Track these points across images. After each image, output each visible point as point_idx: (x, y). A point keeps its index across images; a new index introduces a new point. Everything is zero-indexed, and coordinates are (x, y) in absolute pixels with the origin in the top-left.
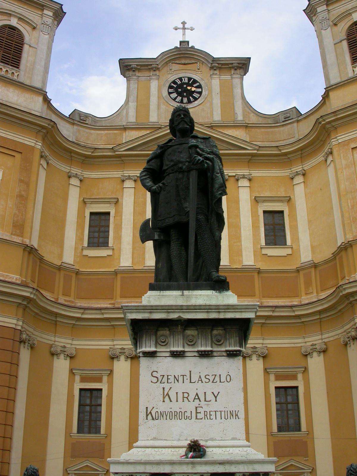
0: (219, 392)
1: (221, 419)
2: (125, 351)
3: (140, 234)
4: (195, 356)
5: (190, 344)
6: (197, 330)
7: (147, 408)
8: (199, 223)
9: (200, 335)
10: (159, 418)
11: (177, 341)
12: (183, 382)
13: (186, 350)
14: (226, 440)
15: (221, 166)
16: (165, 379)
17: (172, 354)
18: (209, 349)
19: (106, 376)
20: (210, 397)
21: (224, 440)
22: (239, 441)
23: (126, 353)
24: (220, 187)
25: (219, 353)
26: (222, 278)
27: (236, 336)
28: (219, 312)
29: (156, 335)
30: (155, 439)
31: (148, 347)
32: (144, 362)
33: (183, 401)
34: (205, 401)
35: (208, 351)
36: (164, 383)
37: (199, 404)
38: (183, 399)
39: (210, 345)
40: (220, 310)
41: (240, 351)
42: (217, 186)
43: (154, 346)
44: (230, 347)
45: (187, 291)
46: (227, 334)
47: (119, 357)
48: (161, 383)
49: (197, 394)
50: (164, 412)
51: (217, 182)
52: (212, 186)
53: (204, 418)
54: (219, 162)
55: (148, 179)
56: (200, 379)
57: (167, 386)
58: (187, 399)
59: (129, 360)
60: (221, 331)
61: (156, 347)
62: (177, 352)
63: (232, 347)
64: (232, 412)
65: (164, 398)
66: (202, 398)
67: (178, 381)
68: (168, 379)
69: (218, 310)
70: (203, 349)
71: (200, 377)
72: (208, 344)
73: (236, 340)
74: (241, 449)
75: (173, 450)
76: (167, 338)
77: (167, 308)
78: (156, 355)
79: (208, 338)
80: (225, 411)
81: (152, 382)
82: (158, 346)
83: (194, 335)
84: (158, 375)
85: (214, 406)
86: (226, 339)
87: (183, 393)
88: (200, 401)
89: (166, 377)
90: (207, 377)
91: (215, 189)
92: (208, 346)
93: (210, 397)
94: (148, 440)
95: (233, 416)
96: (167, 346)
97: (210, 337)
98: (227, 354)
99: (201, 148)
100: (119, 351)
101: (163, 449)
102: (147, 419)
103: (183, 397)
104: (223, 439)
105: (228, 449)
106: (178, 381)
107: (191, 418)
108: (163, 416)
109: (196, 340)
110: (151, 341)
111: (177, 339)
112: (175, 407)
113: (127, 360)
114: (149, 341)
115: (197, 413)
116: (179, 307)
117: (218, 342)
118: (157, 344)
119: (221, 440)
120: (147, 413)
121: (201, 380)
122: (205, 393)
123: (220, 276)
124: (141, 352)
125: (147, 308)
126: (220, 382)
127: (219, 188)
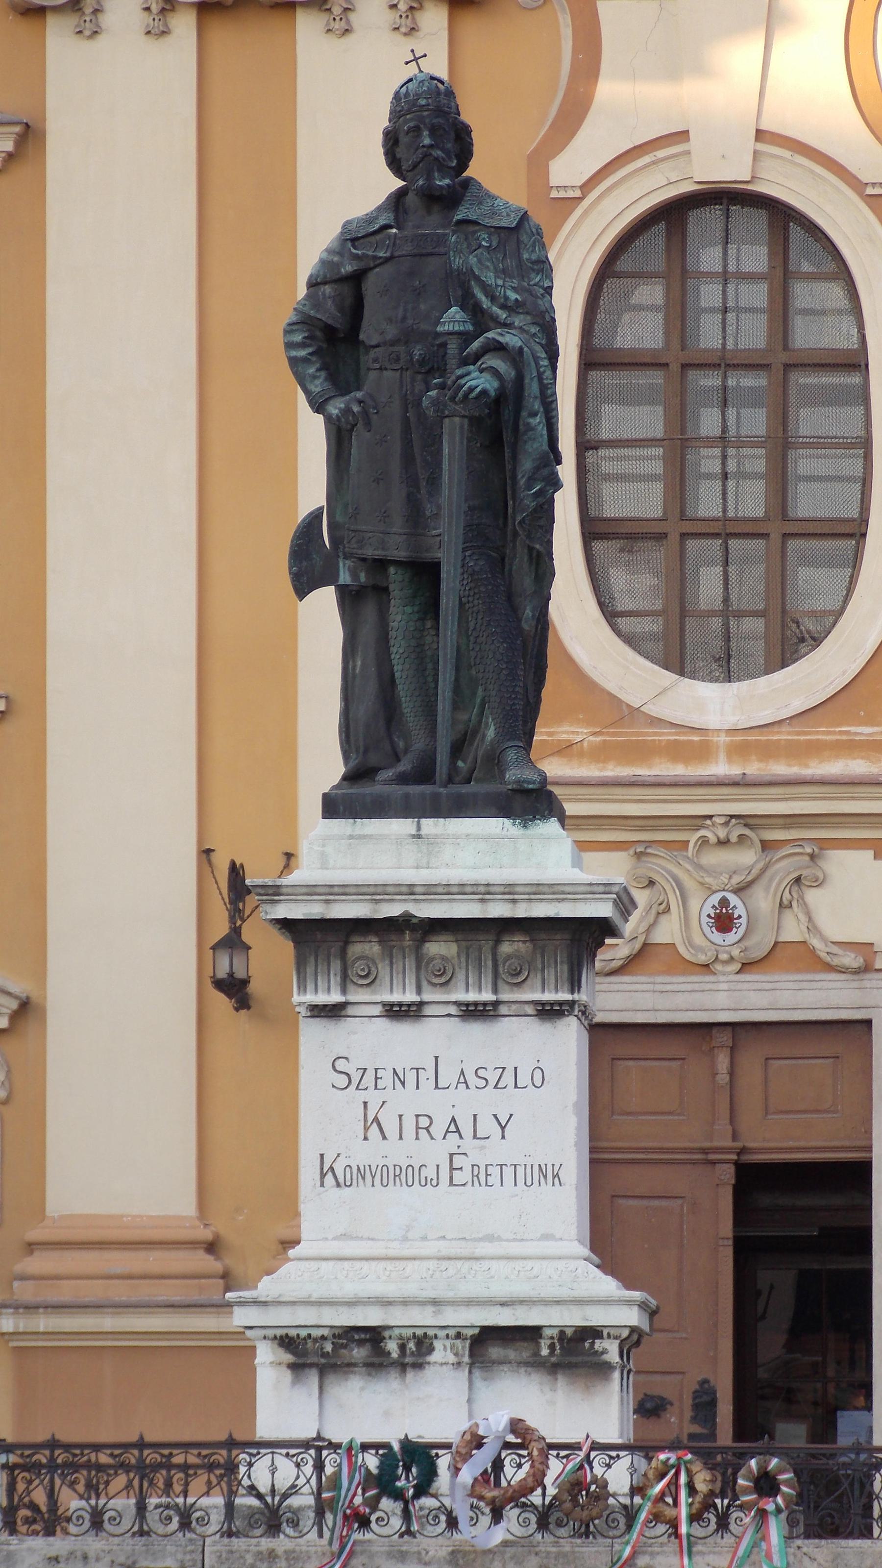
0: (511, 1115)
3: (290, 569)
4: (449, 1015)
6: (456, 941)
14: (527, 1240)
15: (548, 373)
18: (487, 996)
20: (487, 1126)
21: (522, 1240)
24: (537, 469)
25: (514, 1007)
26: (531, 786)
28: (514, 901)
36: (366, 1089)
37: (459, 1147)
38: (417, 1133)
40: (516, 897)
48: (357, 1088)
49: (453, 1119)
54: (544, 355)
57: (374, 1098)
58: (429, 1132)
65: (366, 1129)
66: (466, 1129)
67: (403, 1083)
68: (376, 1078)
69: (511, 897)
70: (472, 996)
71: (462, 1072)
78: (343, 1013)
85: (497, 1151)
87: (417, 1116)
88: (461, 1137)
89: (370, 1074)
90: (481, 1073)
91: (523, 476)
93: (487, 1126)
95: (545, 1177)
96: (373, 987)
102: (322, 1185)
103: (418, 1128)
104: (519, 1237)
105: (529, 1264)
106: (403, 1083)
108: (363, 1178)
112: (397, 1152)
113: (164, 33)
115: (452, 1169)
119: (515, 1240)
121: (466, 1082)
126: (516, 1086)
127: (534, 474)
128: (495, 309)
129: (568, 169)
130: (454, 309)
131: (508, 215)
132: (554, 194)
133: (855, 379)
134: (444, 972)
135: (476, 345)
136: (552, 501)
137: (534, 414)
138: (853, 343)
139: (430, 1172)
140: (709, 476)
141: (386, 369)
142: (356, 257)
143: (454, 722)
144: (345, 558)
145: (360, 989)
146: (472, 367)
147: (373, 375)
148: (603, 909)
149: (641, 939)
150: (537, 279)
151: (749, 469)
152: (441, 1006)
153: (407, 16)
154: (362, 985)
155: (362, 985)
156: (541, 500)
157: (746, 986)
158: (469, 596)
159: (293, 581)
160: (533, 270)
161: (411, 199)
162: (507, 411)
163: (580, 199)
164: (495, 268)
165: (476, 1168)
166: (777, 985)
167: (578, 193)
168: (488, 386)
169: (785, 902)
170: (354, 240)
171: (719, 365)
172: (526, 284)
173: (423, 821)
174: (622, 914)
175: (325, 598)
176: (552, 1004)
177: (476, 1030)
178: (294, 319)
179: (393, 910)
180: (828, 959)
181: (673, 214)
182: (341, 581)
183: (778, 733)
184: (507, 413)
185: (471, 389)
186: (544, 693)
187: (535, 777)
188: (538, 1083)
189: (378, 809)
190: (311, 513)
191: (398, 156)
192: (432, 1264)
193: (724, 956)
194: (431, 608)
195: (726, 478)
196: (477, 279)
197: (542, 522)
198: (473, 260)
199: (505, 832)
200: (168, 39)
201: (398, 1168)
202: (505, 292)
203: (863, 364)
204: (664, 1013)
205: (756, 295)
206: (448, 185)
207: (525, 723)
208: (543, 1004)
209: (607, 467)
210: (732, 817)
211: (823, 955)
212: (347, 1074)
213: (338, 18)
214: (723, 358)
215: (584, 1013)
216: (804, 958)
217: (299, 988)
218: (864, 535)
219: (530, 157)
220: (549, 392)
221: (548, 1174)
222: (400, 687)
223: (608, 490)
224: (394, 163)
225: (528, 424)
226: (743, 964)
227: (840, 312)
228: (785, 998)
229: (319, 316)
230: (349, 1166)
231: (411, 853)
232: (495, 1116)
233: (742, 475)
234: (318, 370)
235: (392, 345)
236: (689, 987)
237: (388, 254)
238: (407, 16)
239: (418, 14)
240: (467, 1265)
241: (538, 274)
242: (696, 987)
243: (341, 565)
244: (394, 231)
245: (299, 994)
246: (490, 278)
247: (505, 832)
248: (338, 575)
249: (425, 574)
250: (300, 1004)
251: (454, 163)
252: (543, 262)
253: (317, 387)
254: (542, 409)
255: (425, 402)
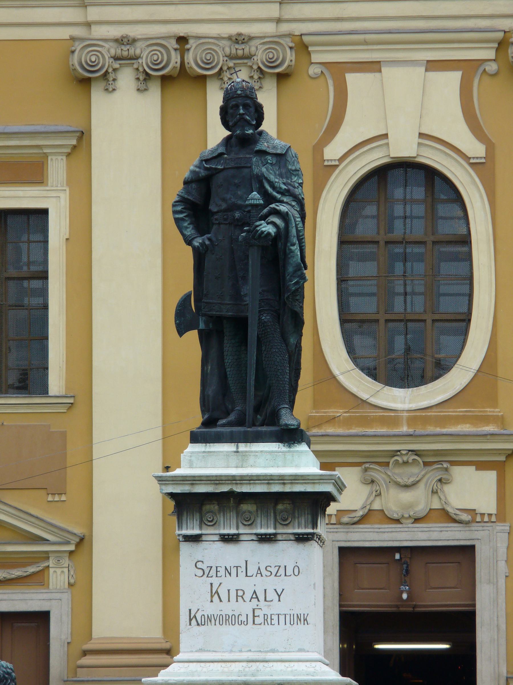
0: (283, 590)
1: (285, 624)
2: (137, 49)
3: (175, 321)
4: (252, 540)
5: (245, 523)
6: (256, 504)
7: (190, 610)
8: (264, 328)
9: (259, 512)
10: (206, 623)
11: (228, 521)
12: (237, 576)
13: (241, 531)
14: (291, 652)
15: (301, 225)
16: (213, 572)
17: (221, 538)
18: (271, 531)
19: (60, 158)
20: (271, 595)
21: (289, 652)
22: (307, 654)
23: (143, 61)
24: (295, 272)
25: (284, 536)
26: (292, 427)
27: (308, 514)
28: (284, 484)
29: (200, 511)
30: (201, 650)
31: (190, 529)
32: (185, 548)
33: (237, 601)
34: (265, 600)
35: (270, 535)
36: (212, 577)
37: (257, 605)
38: (237, 599)
39: (272, 526)
40: (285, 481)
41: (313, 534)
42: (290, 269)
43: (198, 527)
44: (299, 528)
45: (243, 444)
46: (296, 512)
47: (111, 76)
48: (207, 576)
49: (255, 592)
50: (212, 616)
51: (292, 262)
52: (285, 267)
53: (263, 623)
54: (298, 216)
55: (186, 221)
56: (259, 572)
57: (216, 581)
58: (242, 597)
59: (155, 92)
60: (288, 505)
61: (201, 528)
62: (228, 535)
63: (302, 528)
64: (299, 615)
65: (212, 596)
67: (230, 574)
68: (217, 571)
69: (283, 481)
70: (263, 531)
71: (259, 568)
72: (270, 524)
73: (308, 519)
74: (308, 664)
75: (223, 664)
76: (216, 515)
77: (214, 478)
78: (200, 539)
79: (270, 515)
80: (290, 615)
81: (196, 575)
82: (204, 526)
83: (252, 510)
84: (204, 567)
85: (276, 608)
86: (294, 517)
87: (237, 590)
88: (259, 601)
89: (214, 569)
90: (268, 569)
91: (288, 275)
92: (270, 527)
93: (271, 595)
94: (192, 651)
95: (300, 620)
96: (215, 526)
97: (272, 514)
98: (296, 538)
99: (271, 182)
100: (113, 52)
101: (211, 664)
102: (190, 624)
103: (237, 596)
104: (287, 650)
105: (292, 664)
106: (230, 574)
107: (247, 624)
108: (211, 621)
109: (255, 517)
110: (193, 521)
111: (228, 518)
112: (227, 608)
113: (146, 90)
114: (192, 521)
115: (254, 616)
116: (230, 478)
117: (285, 522)
118: (202, 524)
119: (285, 652)
120: (190, 616)
121: (261, 573)
122: (265, 590)
123: (289, 425)
124: (181, 534)
125: (188, 479)
126: (285, 575)
127: (293, 274)
128: (275, 194)
129: (333, 152)
130: (255, 193)
131: (281, 148)
132: (326, 163)
133: (465, 249)
134: (250, 519)
135: (265, 210)
136: (303, 288)
137: (293, 245)
138: (464, 231)
139: (243, 618)
140: (399, 294)
141: (222, 224)
142: (206, 169)
143: (256, 396)
144: (202, 316)
145: (209, 527)
146: (263, 222)
147: (215, 227)
148: (328, 488)
149: (368, 507)
150: (295, 179)
151: (417, 291)
152: (248, 536)
153: (258, 82)
154: (209, 526)
155: (209, 526)
156: (297, 287)
157: (416, 529)
158: (262, 334)
159: (177, 328)
160: (293, 174)
161: (233, 140)
162: (280, 243)
163: (337, 166)
164: (275, 173)
165: (266, 616)
166: (432, 529)
167: (337, 163)
168: (270, 231)
169: (435, 490)
170: (207, 161)
171: (402, 242)
172: (290, 181)
173: (240, 444)
174: (338, 490)
175: (193, 335)
176: (303, 534)
177: (266, 547)
178: (177, 199)
179: (225, 489)
180: (455, 517)
181: (381, 175)
182: (201, 327)
183: (431, 412)
184: (280, 245)
185: (263, 232)
186: (300, 382)
187: (295, 423)
188: (296, 573)
189: (218, 439)
190: (185, 295)
191: (227, 119)
192: (244, 664)
193: (406, 515)
194: (244, 341)
195: (406, 295)
196: (266, 179)
197: (298, 298)
198: (264, 170)
199: (280, 449)
200: (146, 93)
201: (227, 616)
202: (279, 185)
203: (469, 241)
204: (378, 542)
205: (419, 210)
206: (252, 133)
207: (290, 397)
208: (299, 534)
209: (351, 290)
210: (409, 451)
211: (451, 515)
212: (203, 570)
213: (226, 83)
214: (404, 239)
215: (319, 539)
216: (446, 516)
217: (179, 527)
218: (470, 320)
219: (314, 147)
220: (301, 234)
221: (302, 619)
222: (229, 379)
223: (353, 300)
224: (225, 123)
225: (291, 249)
226: (415, 519)
227: (459, 218)
228: (435, 535)
229: (189, 198)
230: (204, 615)
231: (234, 460)
232: (275, 590)
233: (414, 293)
234: (188, 224)
235: (224, 212)
236: (390, 530)
237: (222, 167)
238: (258, 82)
239: (262, 81)
240: (262, 664)
241: (295, 176)
242: (393, 530)
243: (200, 319)
244: (226, 156)
245: (179, 530)
246: (272, 178)
247: (280, 449)
248: (199, 325)
249: (241, 324)
250: (179, 535)
251: (254, 123)
252: (298, 171)
253: (189, 232)
254: (297, 242)
255: (240, 239)
